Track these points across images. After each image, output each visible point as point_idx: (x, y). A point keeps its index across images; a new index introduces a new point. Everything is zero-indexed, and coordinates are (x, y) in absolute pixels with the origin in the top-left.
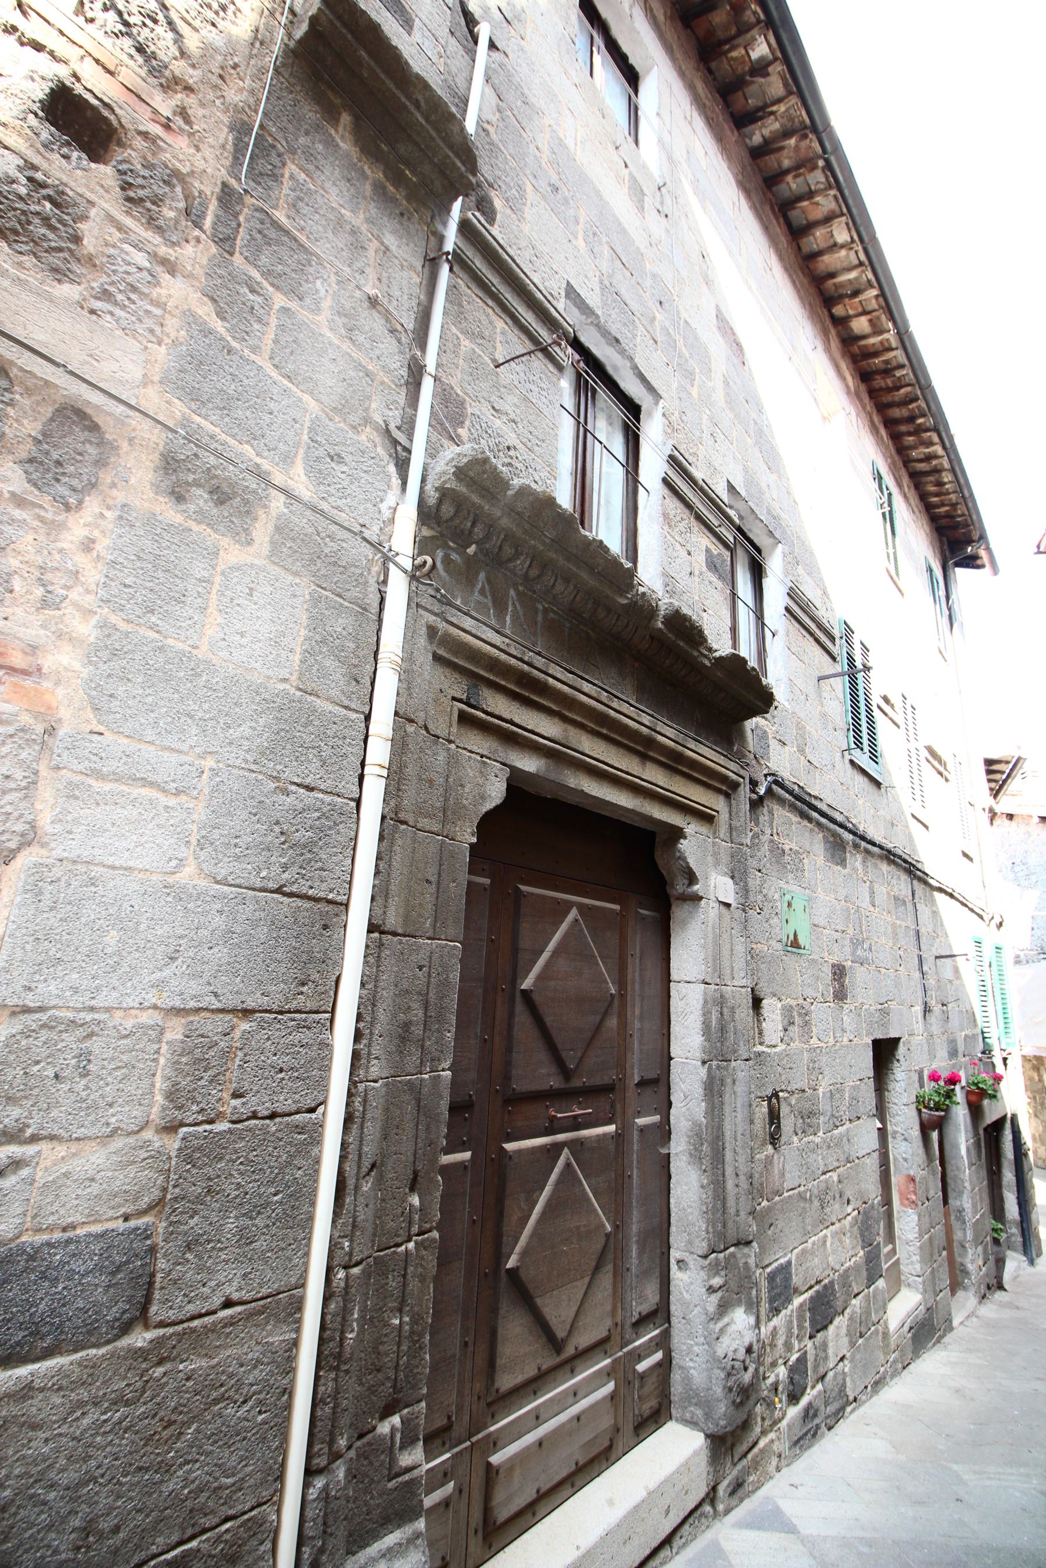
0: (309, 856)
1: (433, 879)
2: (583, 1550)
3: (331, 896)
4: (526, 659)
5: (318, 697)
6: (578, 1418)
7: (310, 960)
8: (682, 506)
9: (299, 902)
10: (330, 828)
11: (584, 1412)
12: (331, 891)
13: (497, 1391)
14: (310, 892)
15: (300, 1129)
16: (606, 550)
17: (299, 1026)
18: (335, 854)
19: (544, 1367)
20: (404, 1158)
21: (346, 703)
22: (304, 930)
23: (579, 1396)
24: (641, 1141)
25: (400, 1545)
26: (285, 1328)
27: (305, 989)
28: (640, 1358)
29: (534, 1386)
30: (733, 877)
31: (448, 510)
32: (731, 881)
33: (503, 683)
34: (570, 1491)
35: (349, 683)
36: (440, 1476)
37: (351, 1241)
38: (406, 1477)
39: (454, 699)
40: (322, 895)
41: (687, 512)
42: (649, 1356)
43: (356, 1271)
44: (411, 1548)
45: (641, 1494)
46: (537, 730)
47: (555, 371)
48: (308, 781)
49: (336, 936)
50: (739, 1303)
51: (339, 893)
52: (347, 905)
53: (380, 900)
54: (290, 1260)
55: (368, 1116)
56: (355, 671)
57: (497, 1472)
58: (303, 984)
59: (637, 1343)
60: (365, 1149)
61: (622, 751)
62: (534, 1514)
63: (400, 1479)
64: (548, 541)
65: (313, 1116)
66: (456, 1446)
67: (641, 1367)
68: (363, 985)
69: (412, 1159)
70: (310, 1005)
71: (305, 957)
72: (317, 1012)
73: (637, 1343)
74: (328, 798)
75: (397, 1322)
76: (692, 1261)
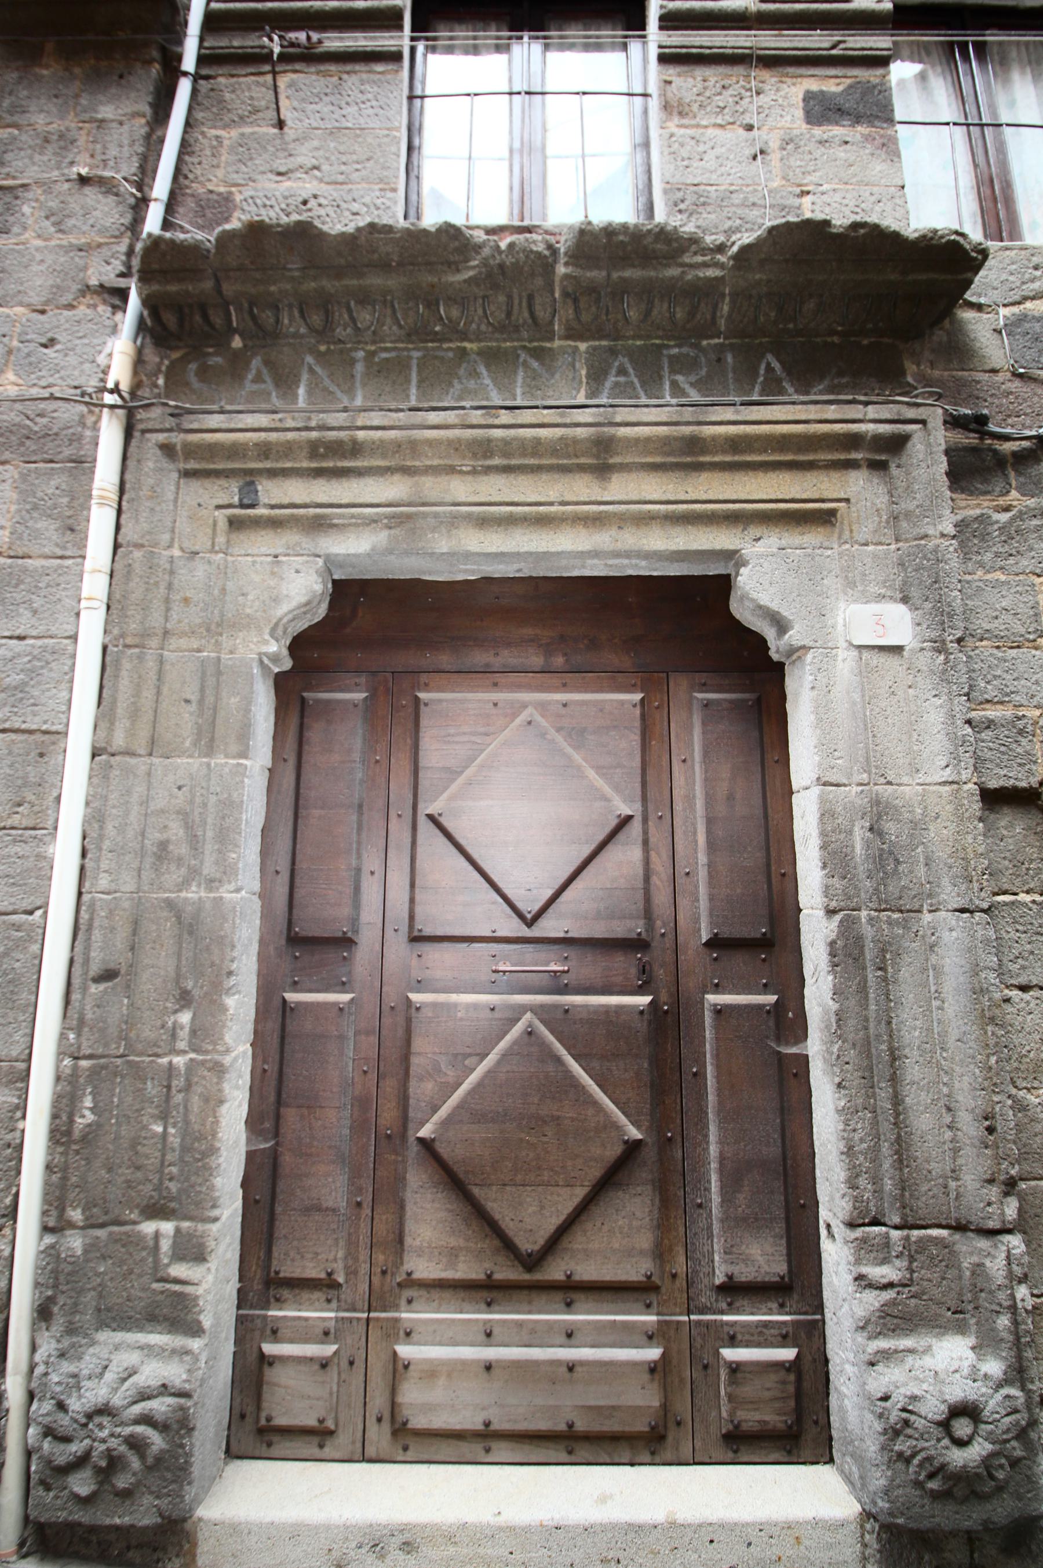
0: (21, 695)
1: (194, 698)
2: (501, 1520)
3: (44, 727)
4: (313, 424)
5: (30, 557)
6: (571, 1368)
7: (25, 784)
8: (722, 69)
9: (13, 736)
10: (42, 667)
11: (583, 1363)
12: (45, 722)
13: (409, 1274)
14: (24, 726)
15: (18, 927)
16: (389, 229)
17: (15, 841)
18: (48, 690)
19: (498, 1276)
20: (162, 973)
21: (60, 553)
22: (19, 759)
23: (573, 1341)
24: (717, 1028)
25: (164, 1350)
26: (7, 1091)
27: (20, 809)
28: (733, 1341)
29: (495, 1294)
30: (905, 600)
31: (170, 319)
32: (902, 608)
33: (331, 464)
34: (564, 1457)
35: (64, 534)
36: (319, 1331)
37: (79, 1035)
38: (177, 1288)
39: (219, 507)
40: (34, 727)
41: (739, 70)
42: (748, 1345)
43: (84, 1063)
44: (177, 1359)
45: (659, 1516)
46: (361, 500)
47: (390, 67)
48: (17, 633)
49: (53, 762)
50: (961, 1329)
51: (53, 724)
52: (66, 734)
53: (103, 725)
54: (11, 1036)
55: (96, 924)
56: (71, 521)
57: (406, 1367)
58: (19, 805)
59: (725, 1318)
60: (93, 954)
61: (544, 477)
62: (488, 1450)
63: (168, 1286)
64: (297, 274)
65: (31, 918)
66: (347, 1310)
67: (729, 1354)
68: (87, 804)
69: (173, 974)
70: (25, 823)
71: (19, 782)
72: (34, 829)
73: (725, 1318)
74: (39, 642)
75: (159, 1129)
76: (839, 1229)
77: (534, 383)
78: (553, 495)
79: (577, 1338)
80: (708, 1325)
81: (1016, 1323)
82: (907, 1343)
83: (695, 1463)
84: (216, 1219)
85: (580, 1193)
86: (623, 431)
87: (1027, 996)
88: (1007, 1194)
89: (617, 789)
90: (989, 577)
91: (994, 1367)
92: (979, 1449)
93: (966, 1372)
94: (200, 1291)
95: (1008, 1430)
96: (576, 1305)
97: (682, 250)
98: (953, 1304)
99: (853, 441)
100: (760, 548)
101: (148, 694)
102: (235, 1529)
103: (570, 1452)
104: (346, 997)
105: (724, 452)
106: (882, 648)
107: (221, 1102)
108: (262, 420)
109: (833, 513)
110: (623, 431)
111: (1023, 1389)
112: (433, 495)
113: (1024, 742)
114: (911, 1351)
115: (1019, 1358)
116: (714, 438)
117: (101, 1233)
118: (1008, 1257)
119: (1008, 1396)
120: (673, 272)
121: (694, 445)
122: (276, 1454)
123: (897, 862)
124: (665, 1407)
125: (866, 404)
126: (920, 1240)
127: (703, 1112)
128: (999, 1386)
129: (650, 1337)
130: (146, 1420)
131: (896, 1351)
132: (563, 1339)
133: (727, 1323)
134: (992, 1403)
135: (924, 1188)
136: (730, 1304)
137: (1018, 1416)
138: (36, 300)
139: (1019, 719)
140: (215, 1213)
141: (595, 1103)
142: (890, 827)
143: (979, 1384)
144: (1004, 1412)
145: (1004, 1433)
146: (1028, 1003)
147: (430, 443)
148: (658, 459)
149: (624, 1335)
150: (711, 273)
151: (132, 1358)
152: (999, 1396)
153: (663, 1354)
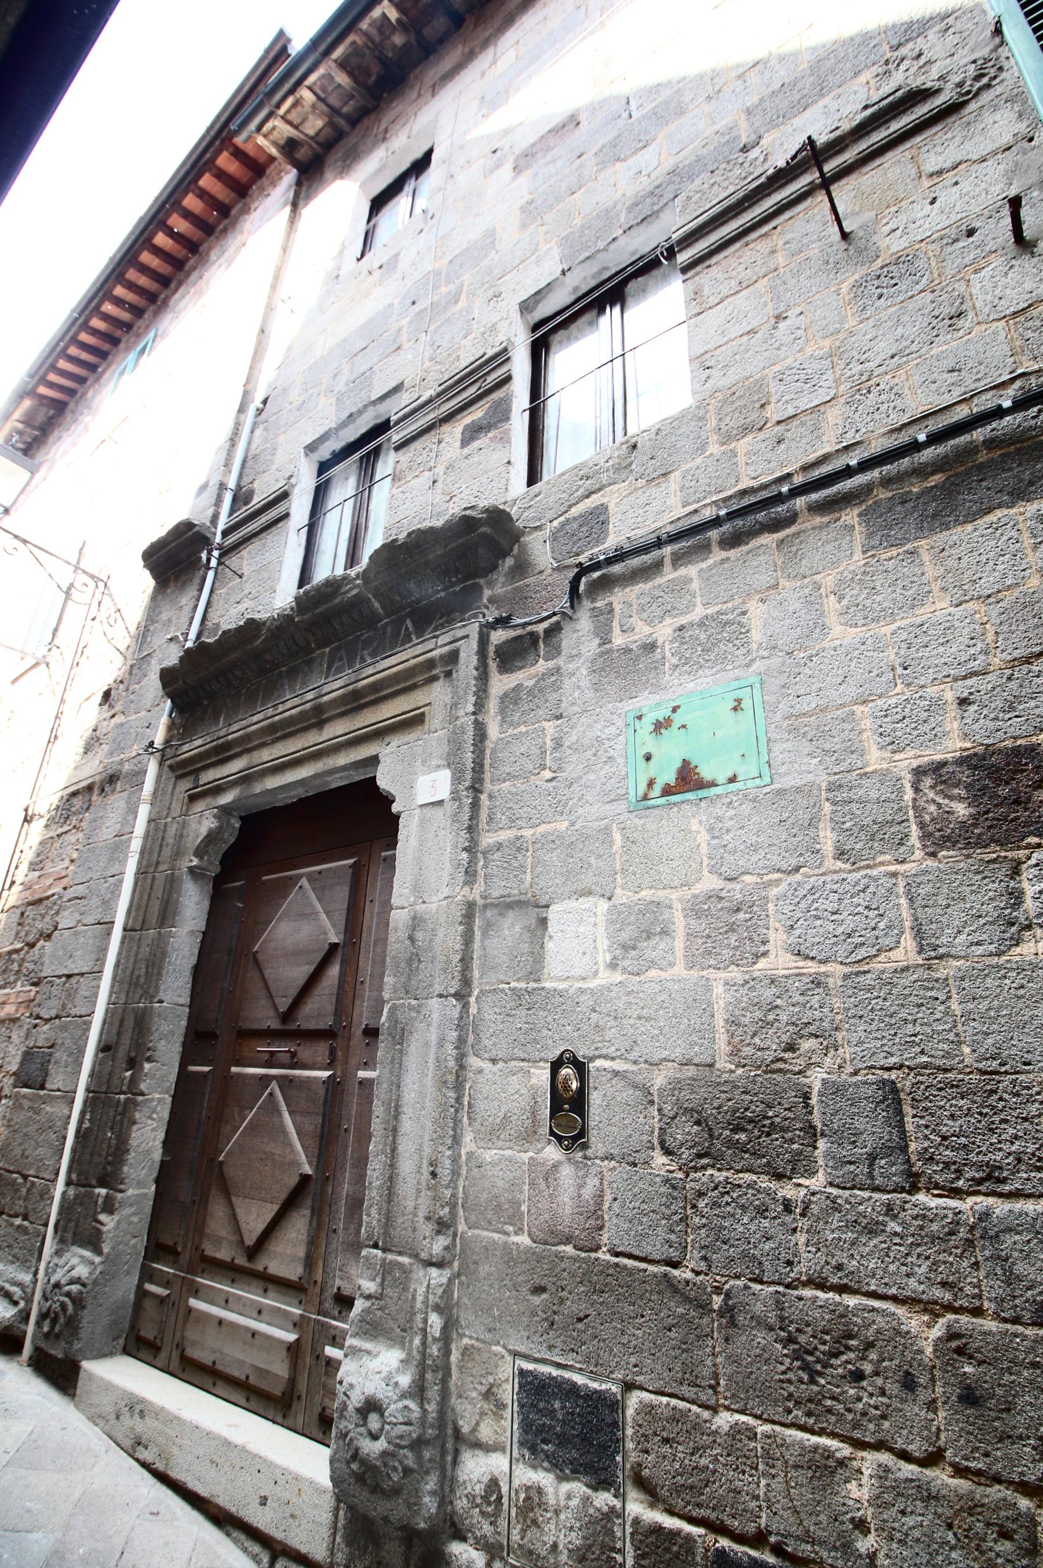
34: (243, 1402)
77: (304, 684)
78: (299, 746)
79: (265, 1316)
80: (323, 1324)
81: (424, 1343)
82: (368, 1345)
83: (303, 1435)
84: (121, 1191)
85: (276, 1208)
86: (326, 698)
87: (495, 1068)
88: (439, 1232)
89: (334, 925)
90: (516, 731)
91: (405, 1380)
92: (381, 1445)
93: (383, 1375)
94: (104, 1229)
95: (401, 1437)
96: (270, 1294)
97: (339, 587)
98: (402, 1321)
99: (431, 664)
100: (389, 749)
101: (145, 897)
102: (91, 1376)
103: (248, 1400)
104: (206, 1069)
105: (371, 694)
106: (432, 804)
107: (134, 1123)
108: (199, 742)
109: (423, 714)
110: (326, 698)
111: (422, 1406)
112: (256, 761)
113: (520, 857)
114: (369, 1353)
115: (422, 1377)
116: (363, 687)
117: (82, 1189)
118: (428, 1286)
119: (406, 1407)
120: (338, 600)
121: (356, 695)
122: (140, 1355)
123: (420, 961)
124: (292, 1381)
125: (436, 637)
126: (391, 1262)
127: (345, 1159)
128: (403, 1396)
129: (295, 1325)
130: (68, 1294)
131: (360, 1350)
132: (255, 1314)
133: (336, 1327)
134: (392, 1407)
135: (400, 1221)
136: (340, 1312)
137: (411, 1428)
138: (148, 706)
139: (518, 839)
140: (122, 1187)
141: (290, 1145)
142: (419, 935)
143: (390, 1388)
144: (401, 1420)
145: (397, 1437)
146: (494, 1074)
147: (254, 732)
148: (343, 709)
149: (279, 1317)
150: (355, 592)
151: (75, 1261)
152: (400, 1405)
153: (298, 1340)
